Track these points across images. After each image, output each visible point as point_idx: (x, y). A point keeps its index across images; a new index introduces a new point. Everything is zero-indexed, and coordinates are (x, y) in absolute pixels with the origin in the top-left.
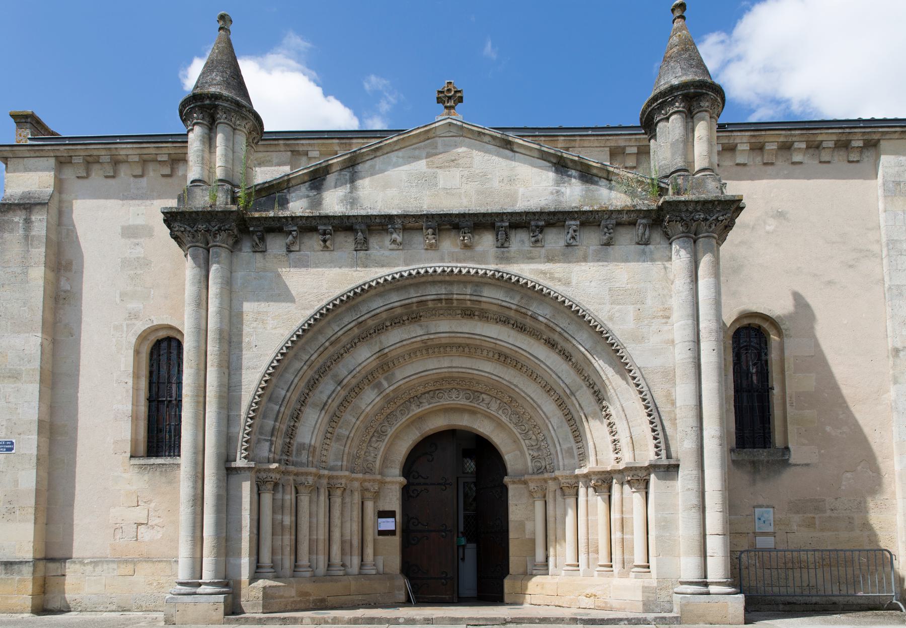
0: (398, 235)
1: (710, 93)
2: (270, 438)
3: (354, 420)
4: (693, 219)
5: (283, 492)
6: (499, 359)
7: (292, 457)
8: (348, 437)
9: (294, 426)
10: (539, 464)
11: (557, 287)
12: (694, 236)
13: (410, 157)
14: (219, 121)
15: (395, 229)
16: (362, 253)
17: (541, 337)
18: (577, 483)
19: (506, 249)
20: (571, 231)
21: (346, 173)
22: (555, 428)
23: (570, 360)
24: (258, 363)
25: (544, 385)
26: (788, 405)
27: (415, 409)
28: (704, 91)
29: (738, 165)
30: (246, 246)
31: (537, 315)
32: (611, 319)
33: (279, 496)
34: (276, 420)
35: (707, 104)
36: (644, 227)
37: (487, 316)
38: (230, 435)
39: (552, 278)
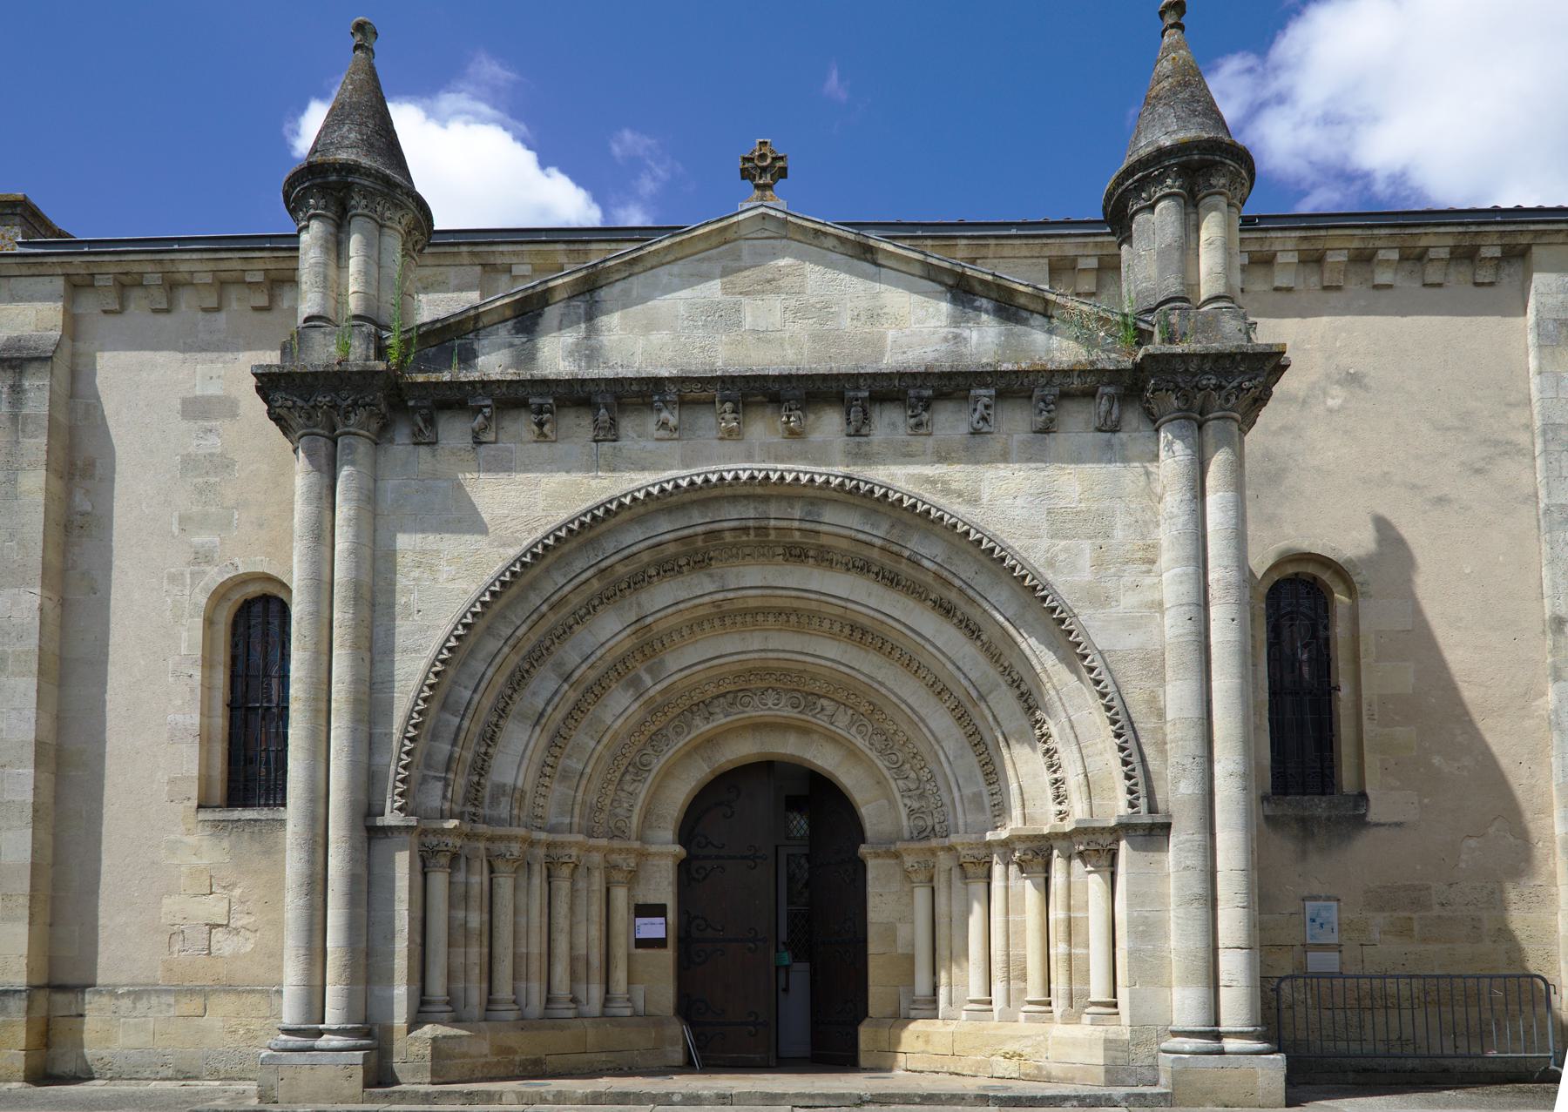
1: (1228, 161)
2: (443, 775)
4: (1196, 386)
5: (468, 871)
8: (582, 774)
10: (921, 823)
12: (1198, 417)
13: (692, 275)
14: (354, 212)
15: (665, 403)
20: (980, 407)
22: (951, 759)
26: (1365, 718)
28: (1217, 158)
30: (402, 435)
31: (919, 557)
32: (1051, 564)
33: (460, 877)
37: (829, 557)
39: (947, 491)
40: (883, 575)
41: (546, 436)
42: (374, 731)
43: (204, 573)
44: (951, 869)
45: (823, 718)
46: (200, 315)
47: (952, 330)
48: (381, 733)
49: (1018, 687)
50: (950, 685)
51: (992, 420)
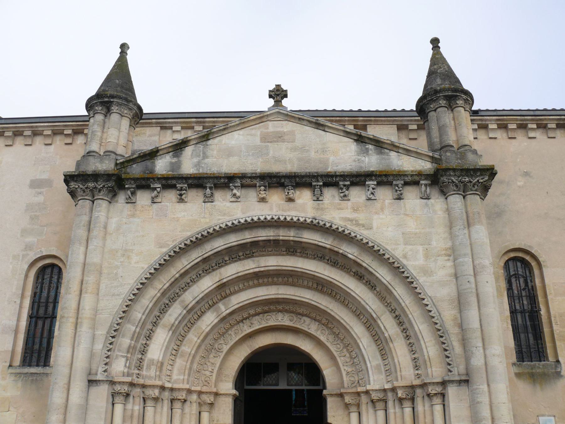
0: (238, 191)
1: (462, 95)
2: (126, 355)
3: (196, 339)
4: (460, 181)
5: (134, 403)
6: (317, 287)
7: (143, 371)
8: (190, 354)
9: (146, 344)
10: (352, 379)
11: (362, 232)
12: (463, 193)
13: (248, 135)
14: (112, 111)
15: (235, 187)
16: (209, 204)
17: (351, 270)
18: (386, 395)
19: (321, 202)
20: (371, 189)
21: (200, 146)
22: (365, 347)
23: (375, 289)
24: (122, 290)
25: (354, 310)
26: (554, 324)
27: (247, 329)
28: (458, 94)
29: (491, 138)
30: (122, 197)
31: (346, 253)
32: (405, 257)
33: (129, 406)
34: (132, 339)
35: (461, 102)
36: (425, 186)
37: (306, 252)
38: (94, 351)
39: (358, 224)
40: (331, 261)
41: (183, 200)
42: (95, 333)
43: (28, 255)
44: (367, 403)
45: (305, 326)
46: (44, 146)
47: (357, 157)
48: (99, 334)
49: (394, 312)
50: (362, 311)
51: (376, 194)
